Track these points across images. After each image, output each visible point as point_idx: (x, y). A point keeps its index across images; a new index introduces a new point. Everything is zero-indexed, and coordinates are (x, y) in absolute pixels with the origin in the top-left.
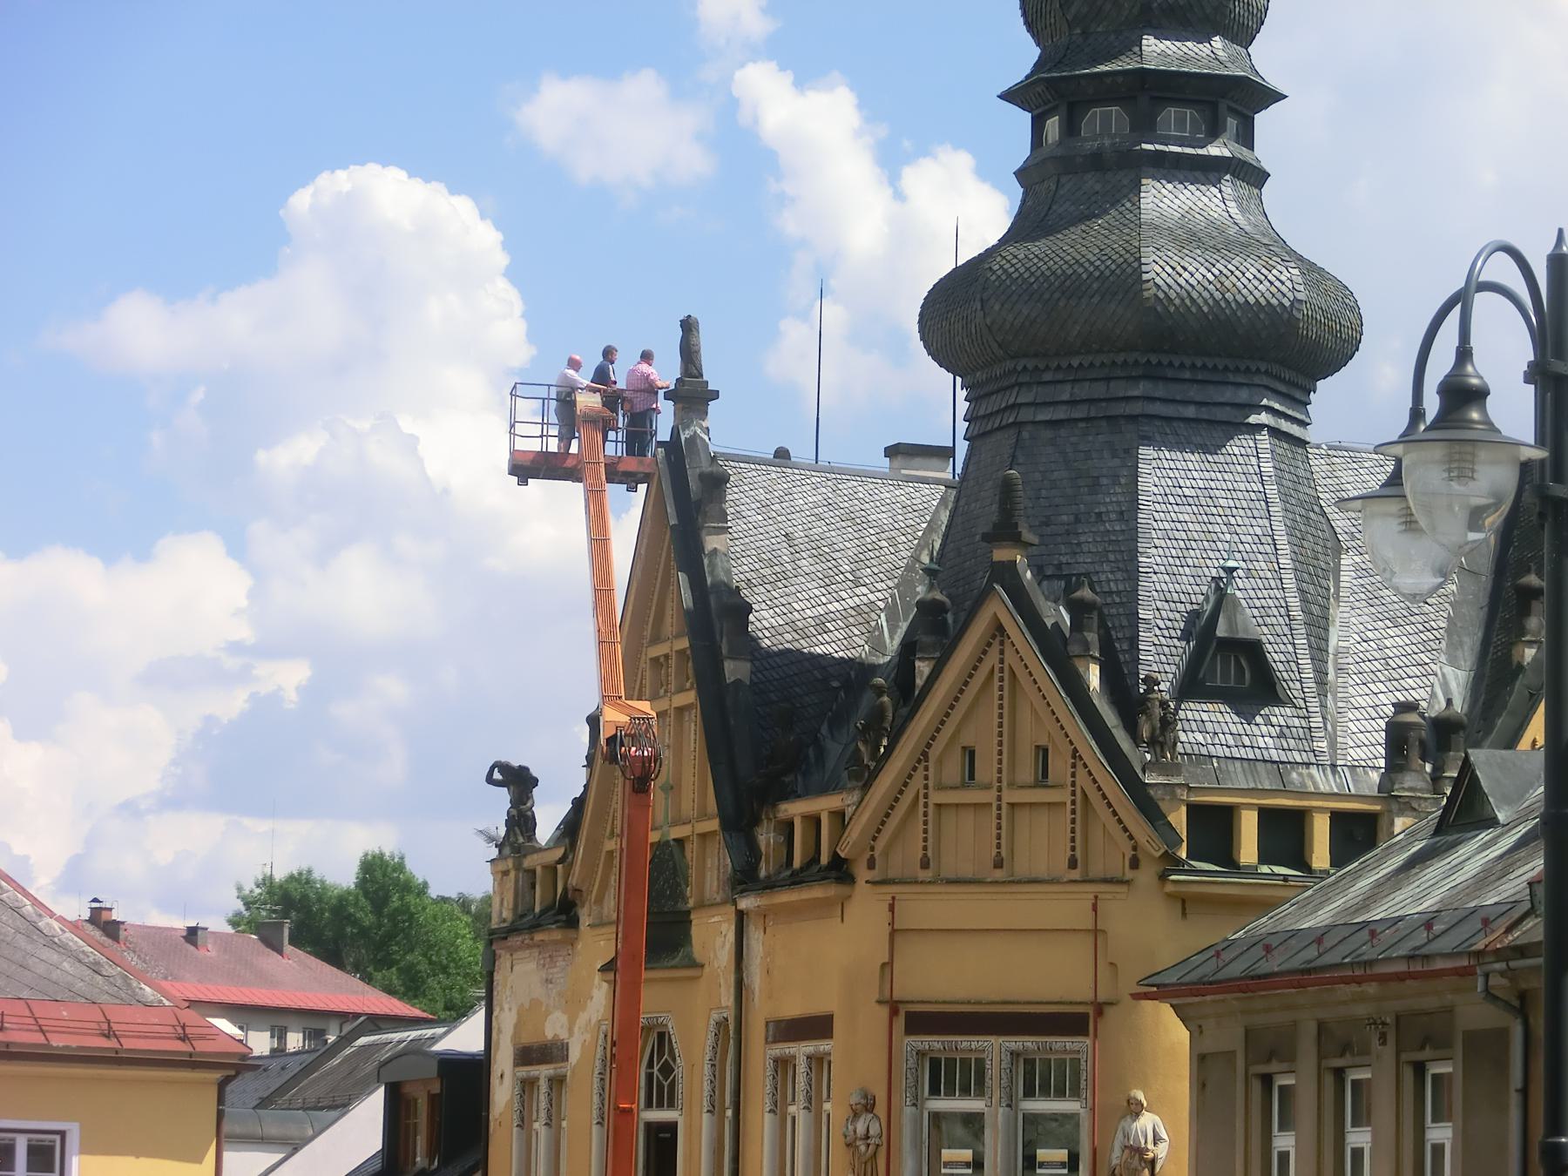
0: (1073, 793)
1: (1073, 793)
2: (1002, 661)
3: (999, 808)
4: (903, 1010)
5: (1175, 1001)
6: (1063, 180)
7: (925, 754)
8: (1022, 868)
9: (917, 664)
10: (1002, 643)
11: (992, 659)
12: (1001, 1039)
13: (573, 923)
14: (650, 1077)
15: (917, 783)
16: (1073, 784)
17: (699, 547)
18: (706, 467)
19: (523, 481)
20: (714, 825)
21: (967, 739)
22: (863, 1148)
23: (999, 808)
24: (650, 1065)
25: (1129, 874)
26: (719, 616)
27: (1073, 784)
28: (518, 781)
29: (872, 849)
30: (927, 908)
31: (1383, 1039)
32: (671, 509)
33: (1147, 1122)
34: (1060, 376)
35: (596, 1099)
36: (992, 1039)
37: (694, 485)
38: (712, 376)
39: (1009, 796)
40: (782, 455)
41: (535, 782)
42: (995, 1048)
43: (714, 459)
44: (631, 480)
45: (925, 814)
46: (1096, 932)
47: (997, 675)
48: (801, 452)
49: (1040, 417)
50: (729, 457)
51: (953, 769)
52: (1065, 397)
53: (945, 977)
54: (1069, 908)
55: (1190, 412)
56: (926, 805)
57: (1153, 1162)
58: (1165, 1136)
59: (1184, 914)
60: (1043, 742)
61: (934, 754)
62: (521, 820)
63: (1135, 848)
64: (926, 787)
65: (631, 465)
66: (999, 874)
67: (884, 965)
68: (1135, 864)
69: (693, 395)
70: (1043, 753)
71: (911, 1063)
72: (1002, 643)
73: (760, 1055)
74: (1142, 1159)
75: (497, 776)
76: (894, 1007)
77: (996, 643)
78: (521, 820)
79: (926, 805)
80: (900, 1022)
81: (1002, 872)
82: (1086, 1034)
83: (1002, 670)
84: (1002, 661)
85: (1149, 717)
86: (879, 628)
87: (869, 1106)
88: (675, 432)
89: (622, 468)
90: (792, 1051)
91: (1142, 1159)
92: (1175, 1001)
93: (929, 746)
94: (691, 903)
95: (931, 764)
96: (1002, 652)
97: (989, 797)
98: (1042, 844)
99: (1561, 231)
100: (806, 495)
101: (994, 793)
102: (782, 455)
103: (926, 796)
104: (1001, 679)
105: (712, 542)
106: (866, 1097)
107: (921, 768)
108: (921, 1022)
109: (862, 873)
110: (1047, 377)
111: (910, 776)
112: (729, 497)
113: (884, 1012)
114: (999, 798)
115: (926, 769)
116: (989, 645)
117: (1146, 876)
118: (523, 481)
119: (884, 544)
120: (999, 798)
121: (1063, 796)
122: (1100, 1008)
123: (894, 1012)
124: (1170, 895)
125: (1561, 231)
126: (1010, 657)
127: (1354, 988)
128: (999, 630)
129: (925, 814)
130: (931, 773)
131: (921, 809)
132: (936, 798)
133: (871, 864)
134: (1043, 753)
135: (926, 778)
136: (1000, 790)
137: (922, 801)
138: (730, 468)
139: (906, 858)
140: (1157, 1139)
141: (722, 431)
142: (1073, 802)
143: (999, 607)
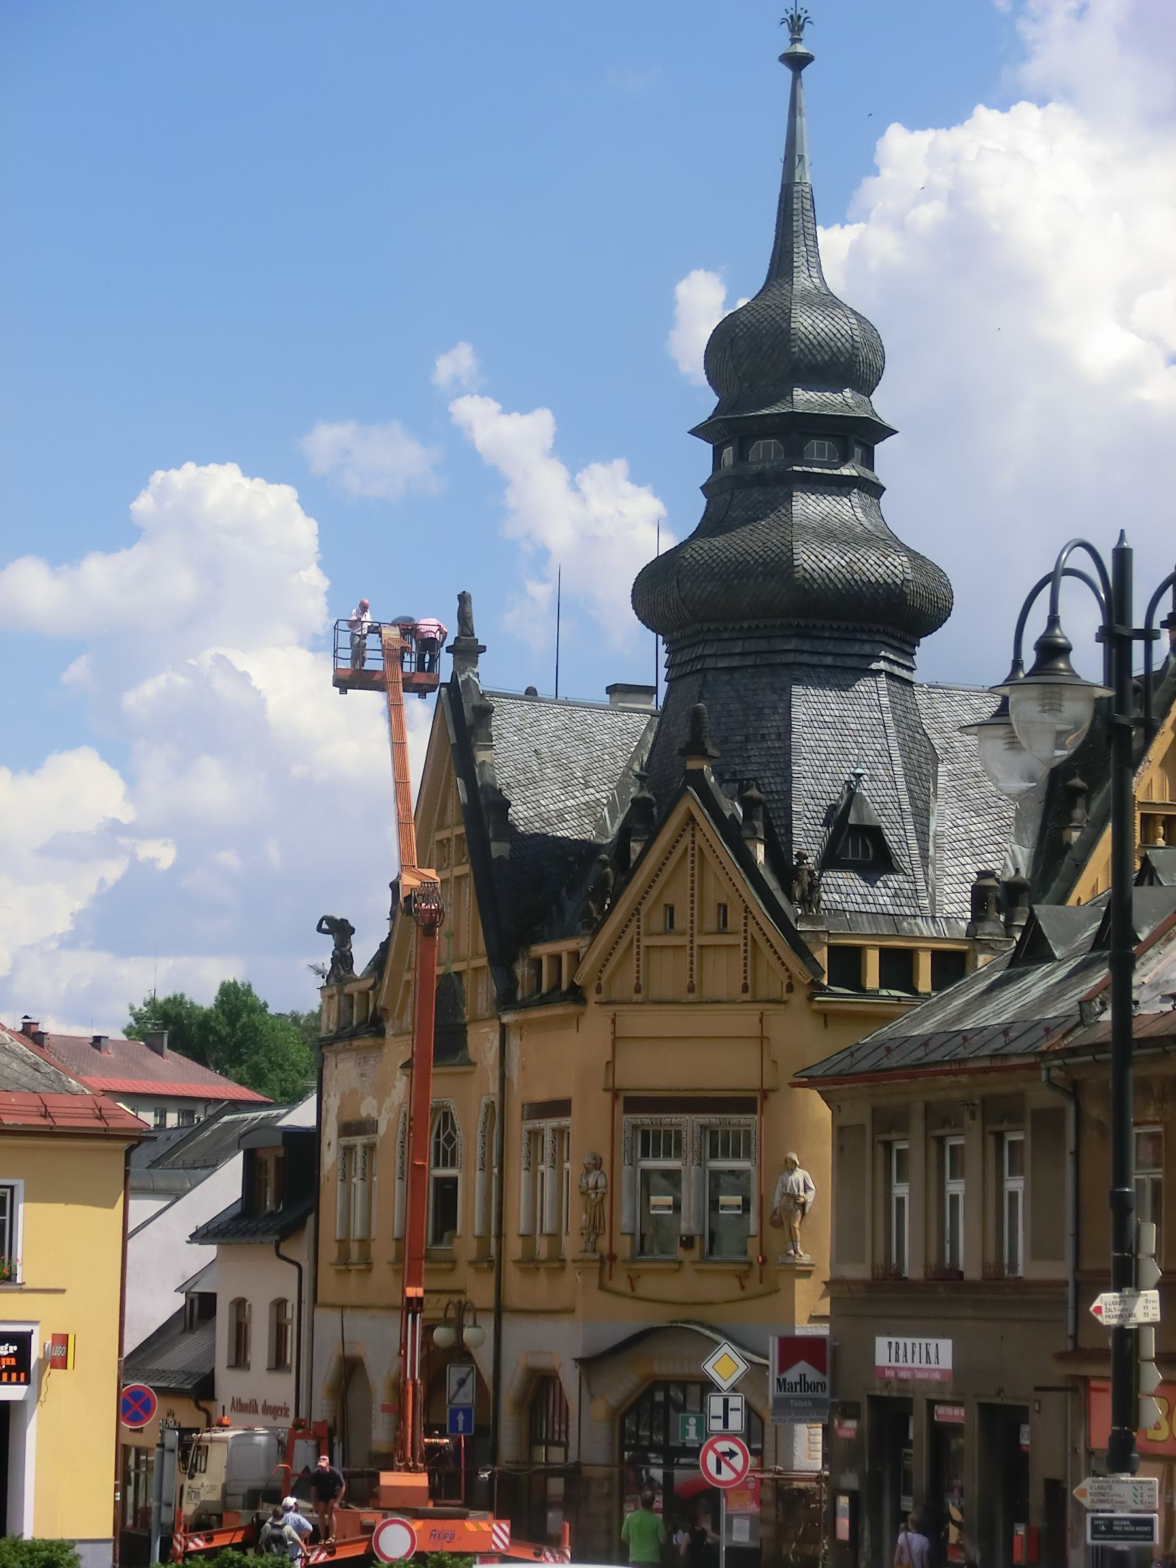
0: (745, 938)
1: (745, 938)
2: (693, 842)
3: (692, 949)
4: (622, 1095)
5: (821, 1089)
6: (736, 493)
7: (638, 910)
8: (708, 992)
9: (632, 844)
10: (693, 829)
11: (686, 840)
12: (693, 1117)
13: (380, 1033)
14: (437, 1144)
15: (632, 931)
16: (745, 931)
17: (472, 759)
18: (477, 702)
19: (344, 691)
20: (483, 961)
21: (668, 901)
22: (593, 1195)
23: (692, 949)
24: (438, 1136)
25: (786, 996)
26: (486, 809)
27: (745, 931)
28: (340, 930)
29: (599, 979)
30: (639, 1022)
31: (973, 1116)
32: (451, 732)
33: (799, 1175)
34: (734, 635)
35: (398, 1161)
36: (687, 1116)
37: (468, 714)
38: (481, 635)
39: (700, 940)
40: (531, 692)
41: (353, 930)
42: (689, 1122)
43: (483, 695)
44: (422, 691)
45: (638, 953)
46: (762, 1038)
47: (690, 852)
48: (545, 690)
49: (720, 665)
50: (493, 694)
51: (658, 920)
52: (738, 650)
53: (651, 1071)
54: (743, 1021)
55: (829, 660)
56: (638, 947)
57: (803, 1205)
58: (812, 1186)
59: (826, 1025)
60: (723, 901)
61: (644, 909)
62: (342, 959)
63: (790, 977)
64: (638, 934)
65: (421, 678)
66: (692, 997)
67: (608, 1063)
68: (790, 989)
69: (467, 650)
70: (723, 908)
71: (628, 1134)
72: (693, 829)
73: (518, 1128)
74: (795, 1203)
75: (325, 926)
76: (615, 1093)
77: (689, 832)
78: (342, 959)
79: (638, 947)
80: (620, 1105)
81: (694, 996)
82: (754, 1112)
83: (693, 849)
84: (693, 842)
85: (800, 882)
86: (603, 818)
87: (598, 1165)
88: (454, 676)
89: (415, 680)
90: (542, 1125)
91: (795, 1203)
92: (821, 1089)
93: (640, 904)
94: (467, 1018)
95: (642, 917)
96: (693, 836)
97: (684, 940)
98: (723, 975)
99: (464, 599)
100: (551, 721)
101: (688, 938)
102: (531, 692)
103: (638, 940)
104: (693, 855)
105: (481, 756)
106: (595, 1158)
107: (634, 919)
108: (636, 1104)
109: (592, 997)
110: (726, 635)
111: (627, 926)
112: (493, 723)
113: (608, 1097)
114: (692, 942)
115: (639, 920)
116: (684, 830)
117: (798, 998)
118: (344, 691)
119: (606, 757)
120: (692, 942)
121: (738, 940)
122: (765, 1093)
123: (615, 1097)
124: (814, 1011)
125: (464, 599)
126: (698, 835)
127: (952, 1078)
128: (691, 819)
129: (638, 953)
130: (642, 923)
131: (635, 950)
132: (646, 941)
133: (599, 990)
134: (723, 908)
135: (639, 927)
136: (692, 935)
137: (635, 943)
138: (495, 702)
139: (624, 986)
140: (806, 1188)
141: (489, 675)
142: (745, 945)
143: (691, 802)
